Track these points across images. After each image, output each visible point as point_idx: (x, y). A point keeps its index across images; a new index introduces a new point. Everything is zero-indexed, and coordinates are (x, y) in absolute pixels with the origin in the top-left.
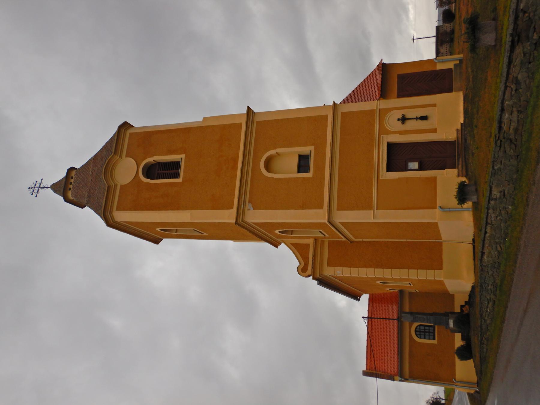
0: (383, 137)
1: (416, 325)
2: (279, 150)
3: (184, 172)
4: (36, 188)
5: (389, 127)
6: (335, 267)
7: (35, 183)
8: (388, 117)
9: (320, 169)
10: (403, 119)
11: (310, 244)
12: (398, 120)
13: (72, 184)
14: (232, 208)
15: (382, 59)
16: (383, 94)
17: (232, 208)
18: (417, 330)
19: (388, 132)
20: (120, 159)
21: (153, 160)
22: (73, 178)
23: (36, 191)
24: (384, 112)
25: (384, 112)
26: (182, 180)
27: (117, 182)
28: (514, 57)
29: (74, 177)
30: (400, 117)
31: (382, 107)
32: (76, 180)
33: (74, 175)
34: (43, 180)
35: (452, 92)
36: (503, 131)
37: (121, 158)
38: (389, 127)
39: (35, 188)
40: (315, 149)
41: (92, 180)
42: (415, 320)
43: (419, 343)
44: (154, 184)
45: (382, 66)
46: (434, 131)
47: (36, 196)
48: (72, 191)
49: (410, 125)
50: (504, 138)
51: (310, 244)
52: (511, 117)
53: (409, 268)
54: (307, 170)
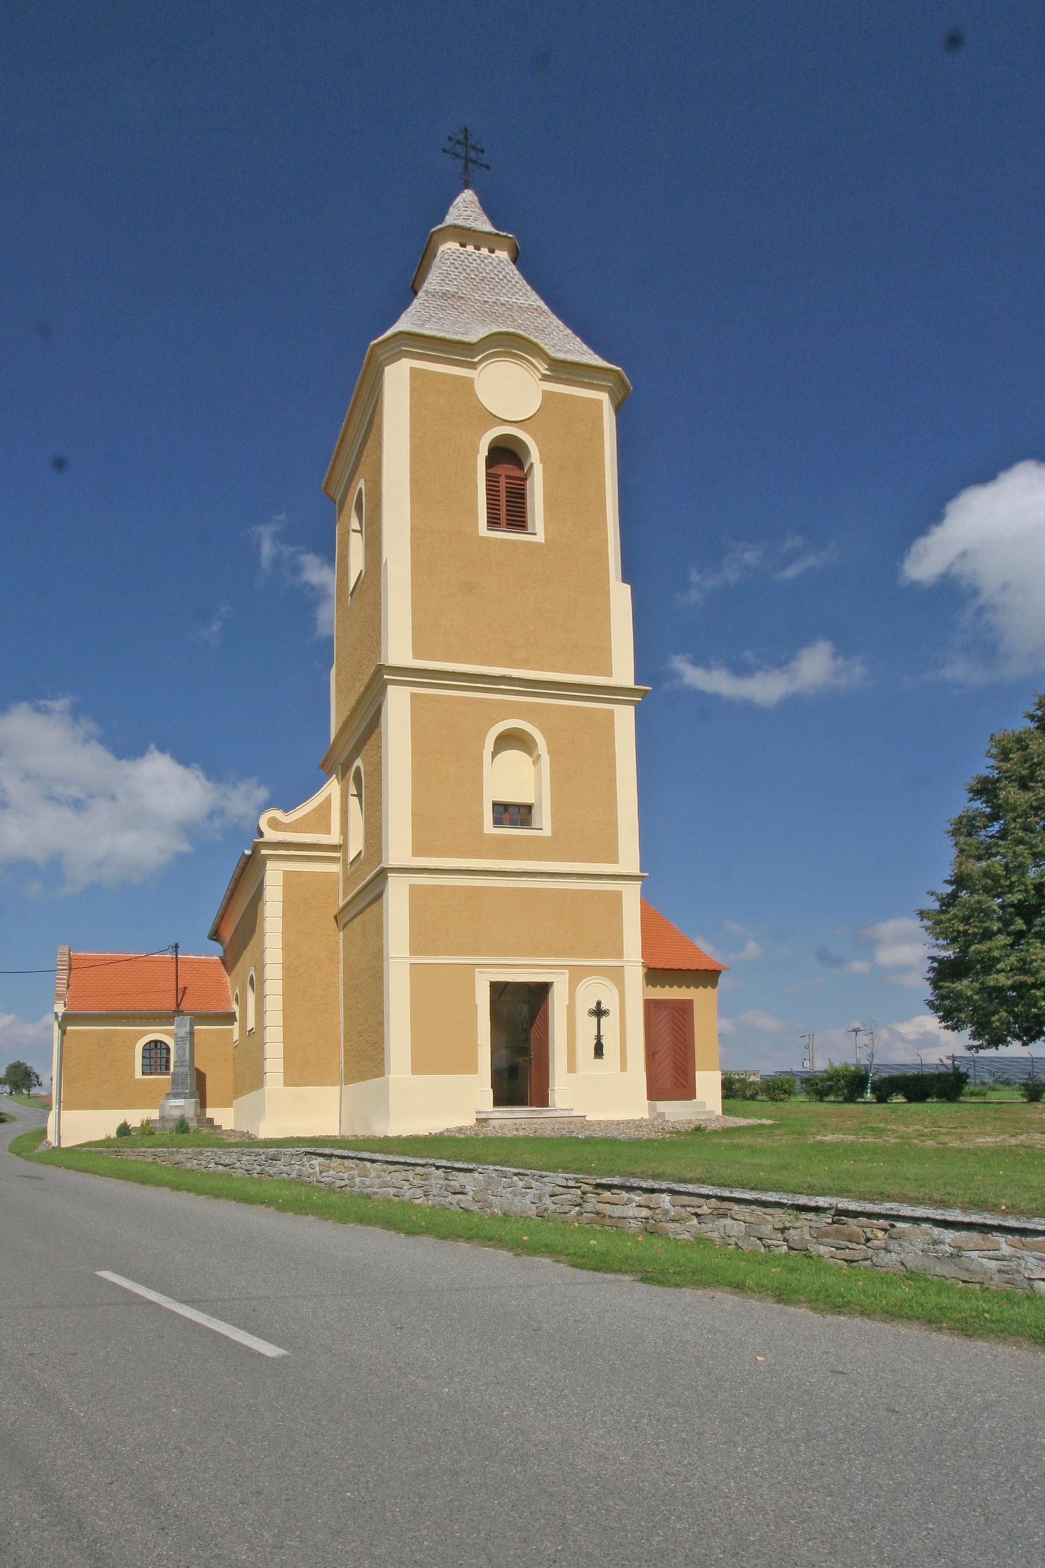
0: (563, 974)
1: (170, 1042)
2: (545, 759)
3: (503, 541)
4: (466, 150)
5: (583, 988)
6: (283, 886)
7: (479, 146)
8: (607, 984)
9: (502, 849)
10: (599, 1012)
11: (330, 834)
12: (599, 1004)
13: (476, 251)
14: (416, 656)
15: (729, 969)
16: (654, 975)
17: (416, 656)
18: (159, 1044)
19: (573, 984)
20: (540, 377)
21: (533, 461)
22: (490, 254)
23: (459, 149)
24: (616, 976)
25: (616, 976)
26: (484, 535)
27: (482, 370)
28: (615, 1191)
29: (493, 255)
30: (604, 1006)
31: (628, 971)
32: (486, 261)
33: (497, 257)
34: (485, 169)
35: (648, 1099)
36: (600, 1192)
37: (540, 380)
38: (586, 985)
39: (466, 146)
40: (543, 839)
41: (486, 302)
42: (178, 1040)
43: (134, 1048)
44: (475, 467)
45: (714, 971)
46: (572, 1068)
47: (444, 151)
48: (458, 250)
49: (587, 1026)
50: (584, 1193)
51: (330, 834)
52: (634, 1204)
53: (285, 1026)
54: (498, 822)
